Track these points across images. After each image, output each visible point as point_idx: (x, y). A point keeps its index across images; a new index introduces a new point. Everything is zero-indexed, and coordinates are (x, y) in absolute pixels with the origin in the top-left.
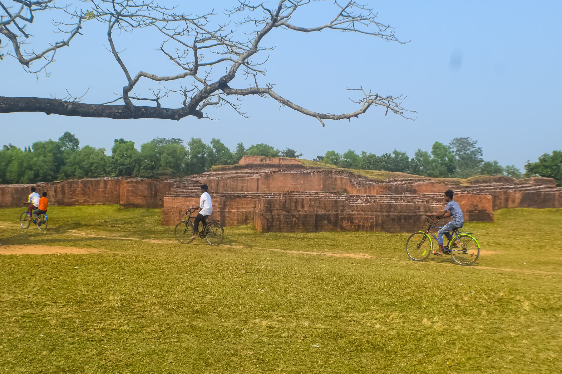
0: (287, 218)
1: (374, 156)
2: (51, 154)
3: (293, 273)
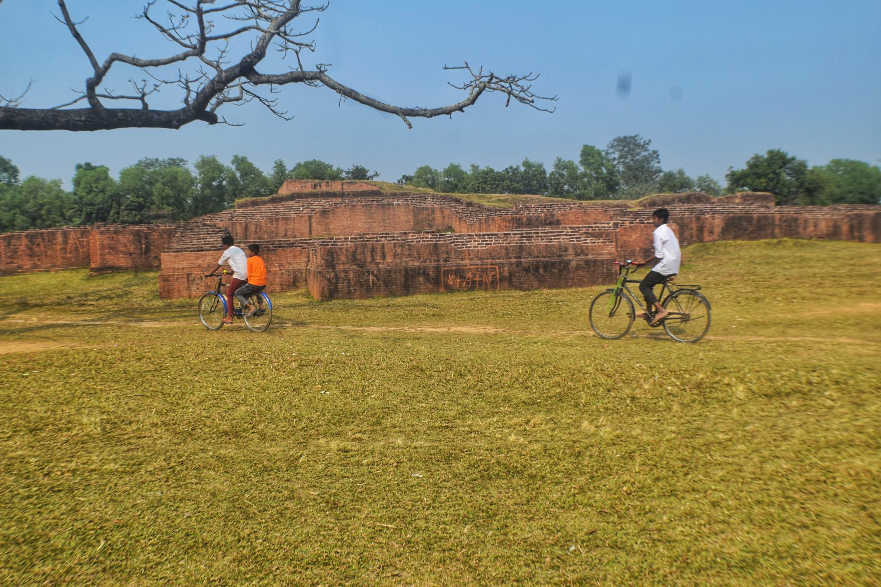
0: (354, 279)
1: (492, 171)
3: (375, 362)
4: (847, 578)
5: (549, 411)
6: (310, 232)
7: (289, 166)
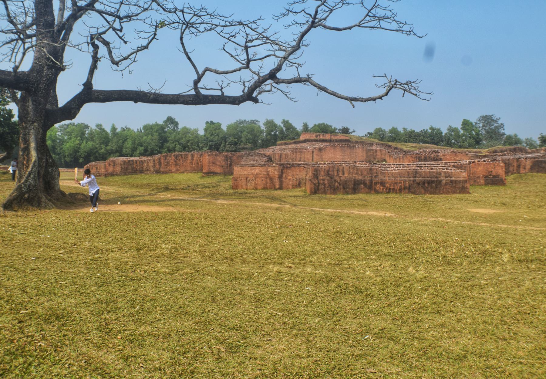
0: (327, 184)
1: (414, 131)
2: (157, 134)
4: (514, 373)
5: (396, 260)
7: (310, 126)
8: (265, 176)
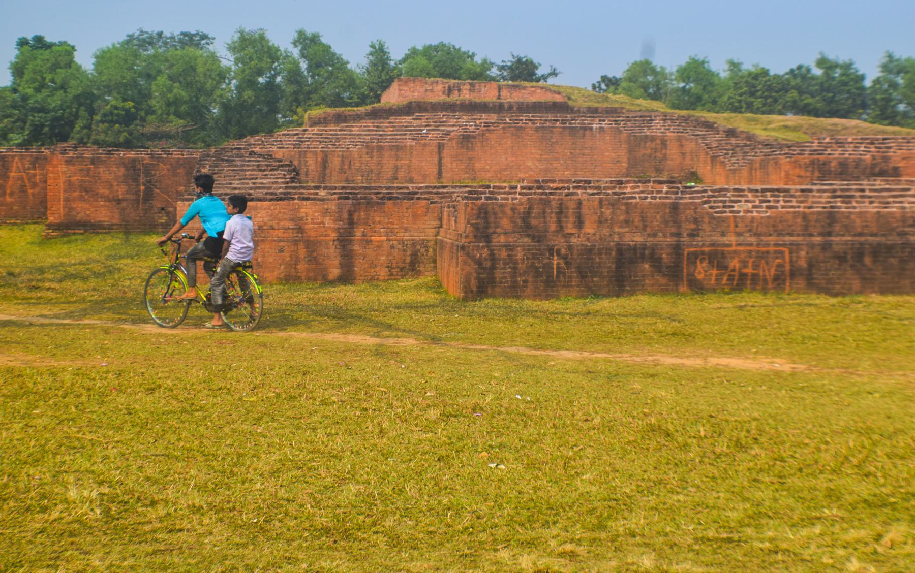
0: (526, 259)
1: (765, 73)
3: (579, 415)
6: (440, 173)
8: (290, 234)
